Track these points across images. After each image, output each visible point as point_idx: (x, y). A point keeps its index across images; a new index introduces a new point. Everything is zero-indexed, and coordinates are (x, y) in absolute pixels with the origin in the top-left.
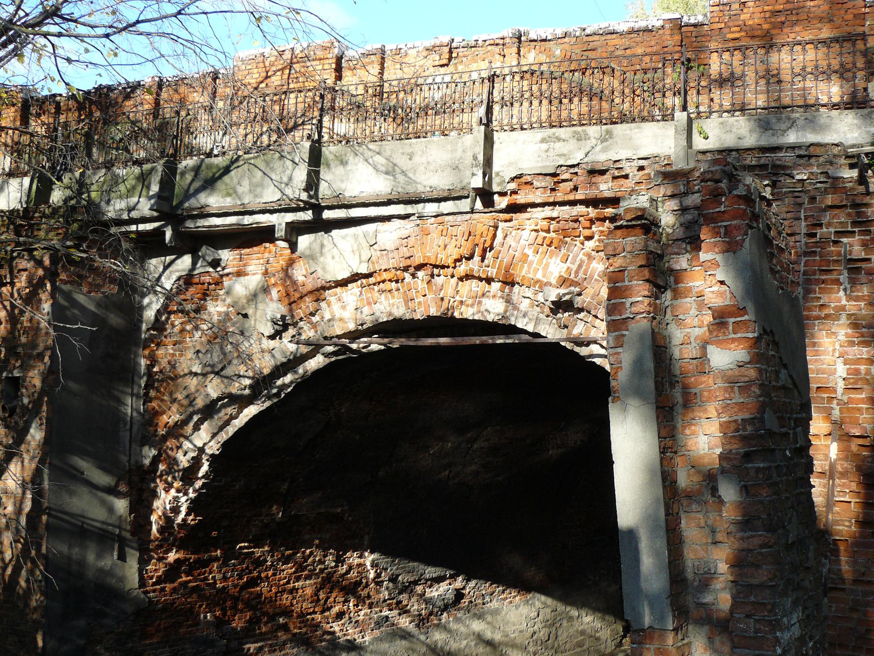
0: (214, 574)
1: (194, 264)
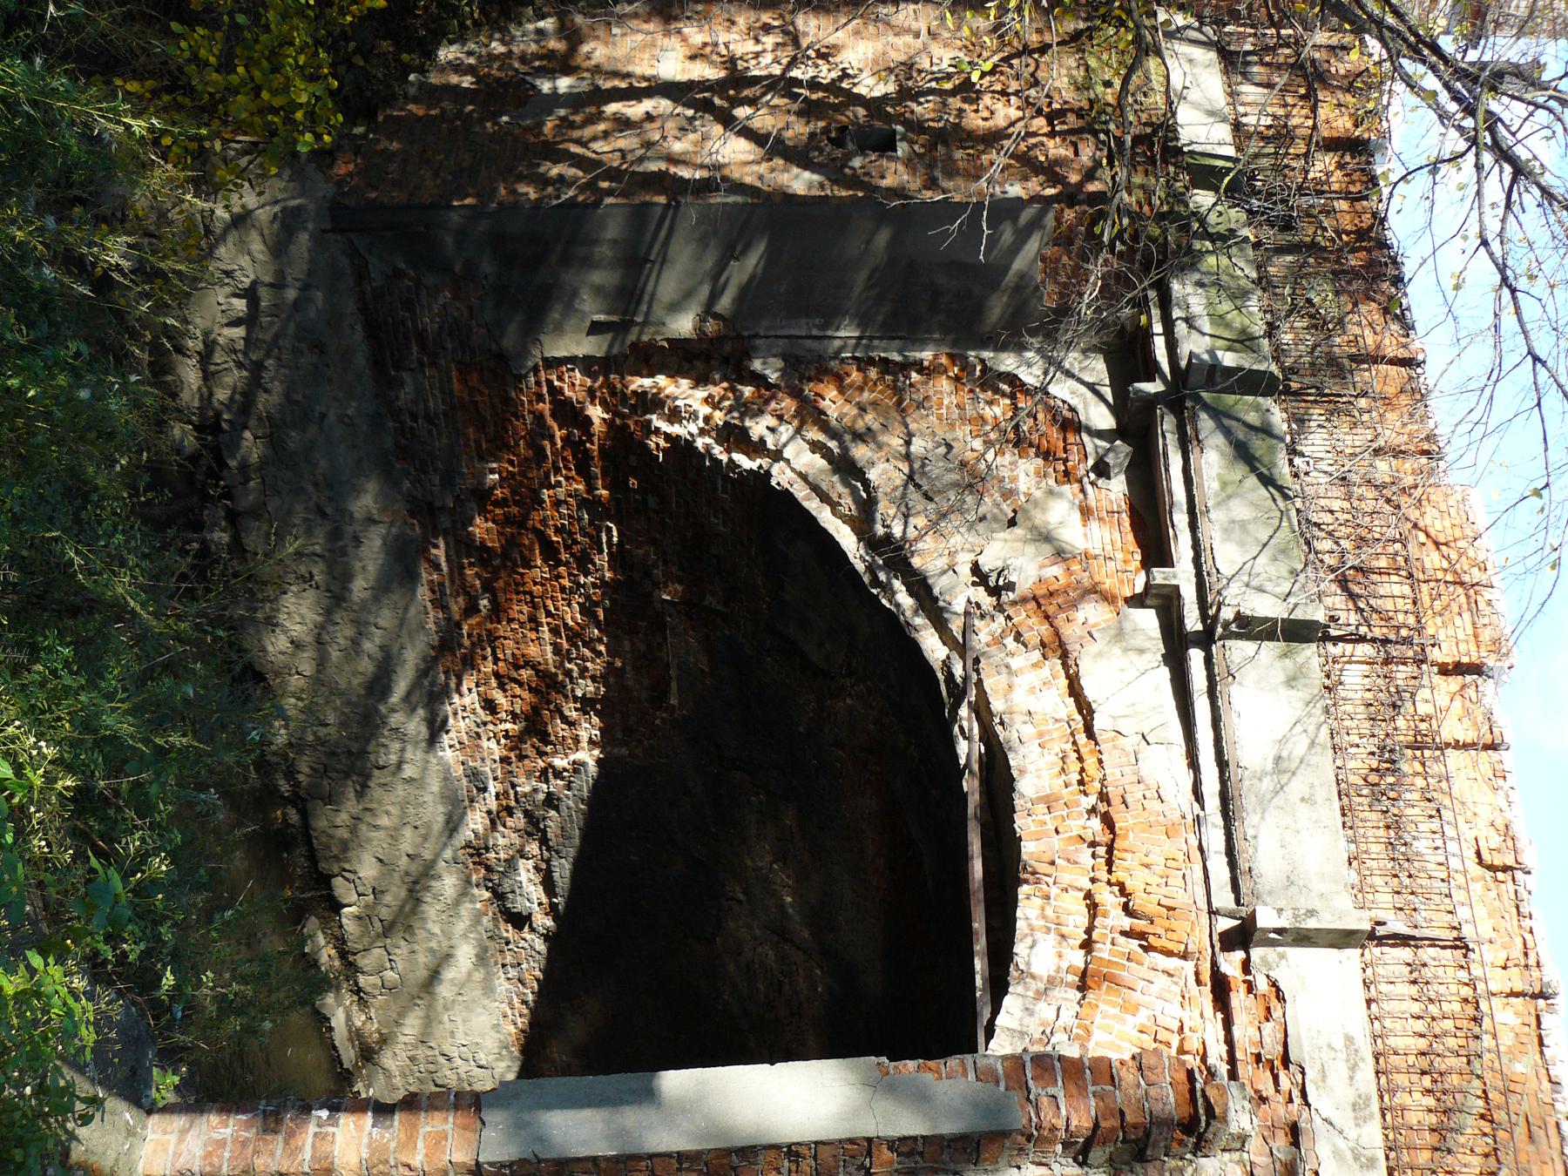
0: (567, 485)
1: (1100, 434)
